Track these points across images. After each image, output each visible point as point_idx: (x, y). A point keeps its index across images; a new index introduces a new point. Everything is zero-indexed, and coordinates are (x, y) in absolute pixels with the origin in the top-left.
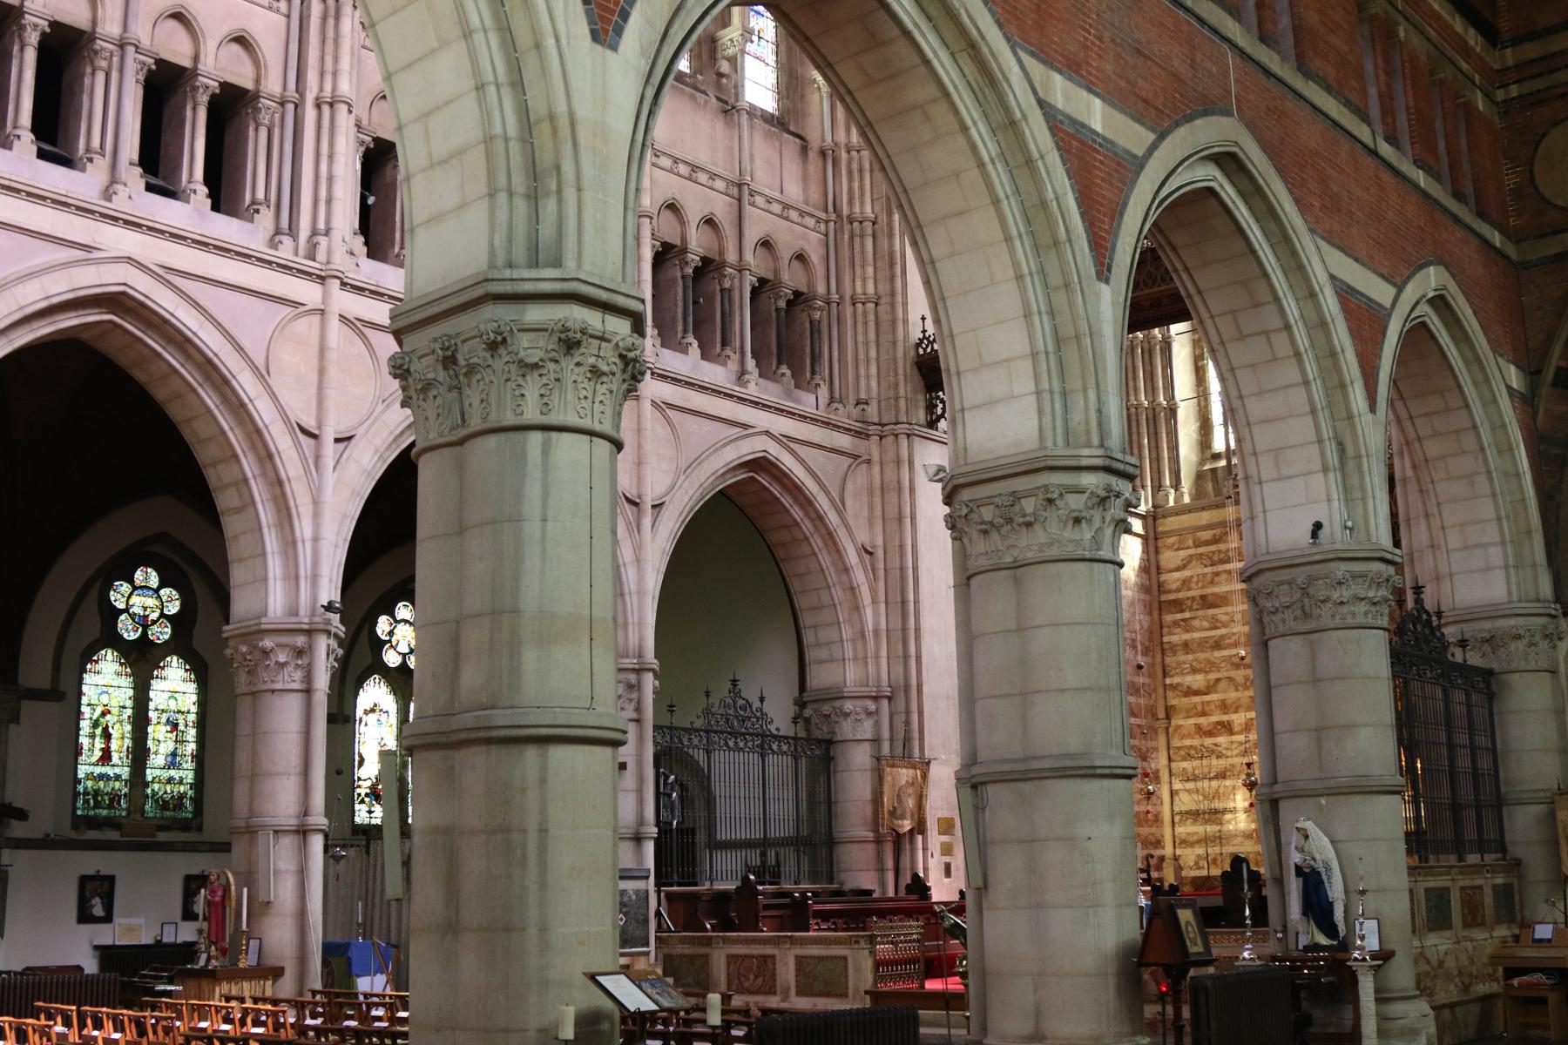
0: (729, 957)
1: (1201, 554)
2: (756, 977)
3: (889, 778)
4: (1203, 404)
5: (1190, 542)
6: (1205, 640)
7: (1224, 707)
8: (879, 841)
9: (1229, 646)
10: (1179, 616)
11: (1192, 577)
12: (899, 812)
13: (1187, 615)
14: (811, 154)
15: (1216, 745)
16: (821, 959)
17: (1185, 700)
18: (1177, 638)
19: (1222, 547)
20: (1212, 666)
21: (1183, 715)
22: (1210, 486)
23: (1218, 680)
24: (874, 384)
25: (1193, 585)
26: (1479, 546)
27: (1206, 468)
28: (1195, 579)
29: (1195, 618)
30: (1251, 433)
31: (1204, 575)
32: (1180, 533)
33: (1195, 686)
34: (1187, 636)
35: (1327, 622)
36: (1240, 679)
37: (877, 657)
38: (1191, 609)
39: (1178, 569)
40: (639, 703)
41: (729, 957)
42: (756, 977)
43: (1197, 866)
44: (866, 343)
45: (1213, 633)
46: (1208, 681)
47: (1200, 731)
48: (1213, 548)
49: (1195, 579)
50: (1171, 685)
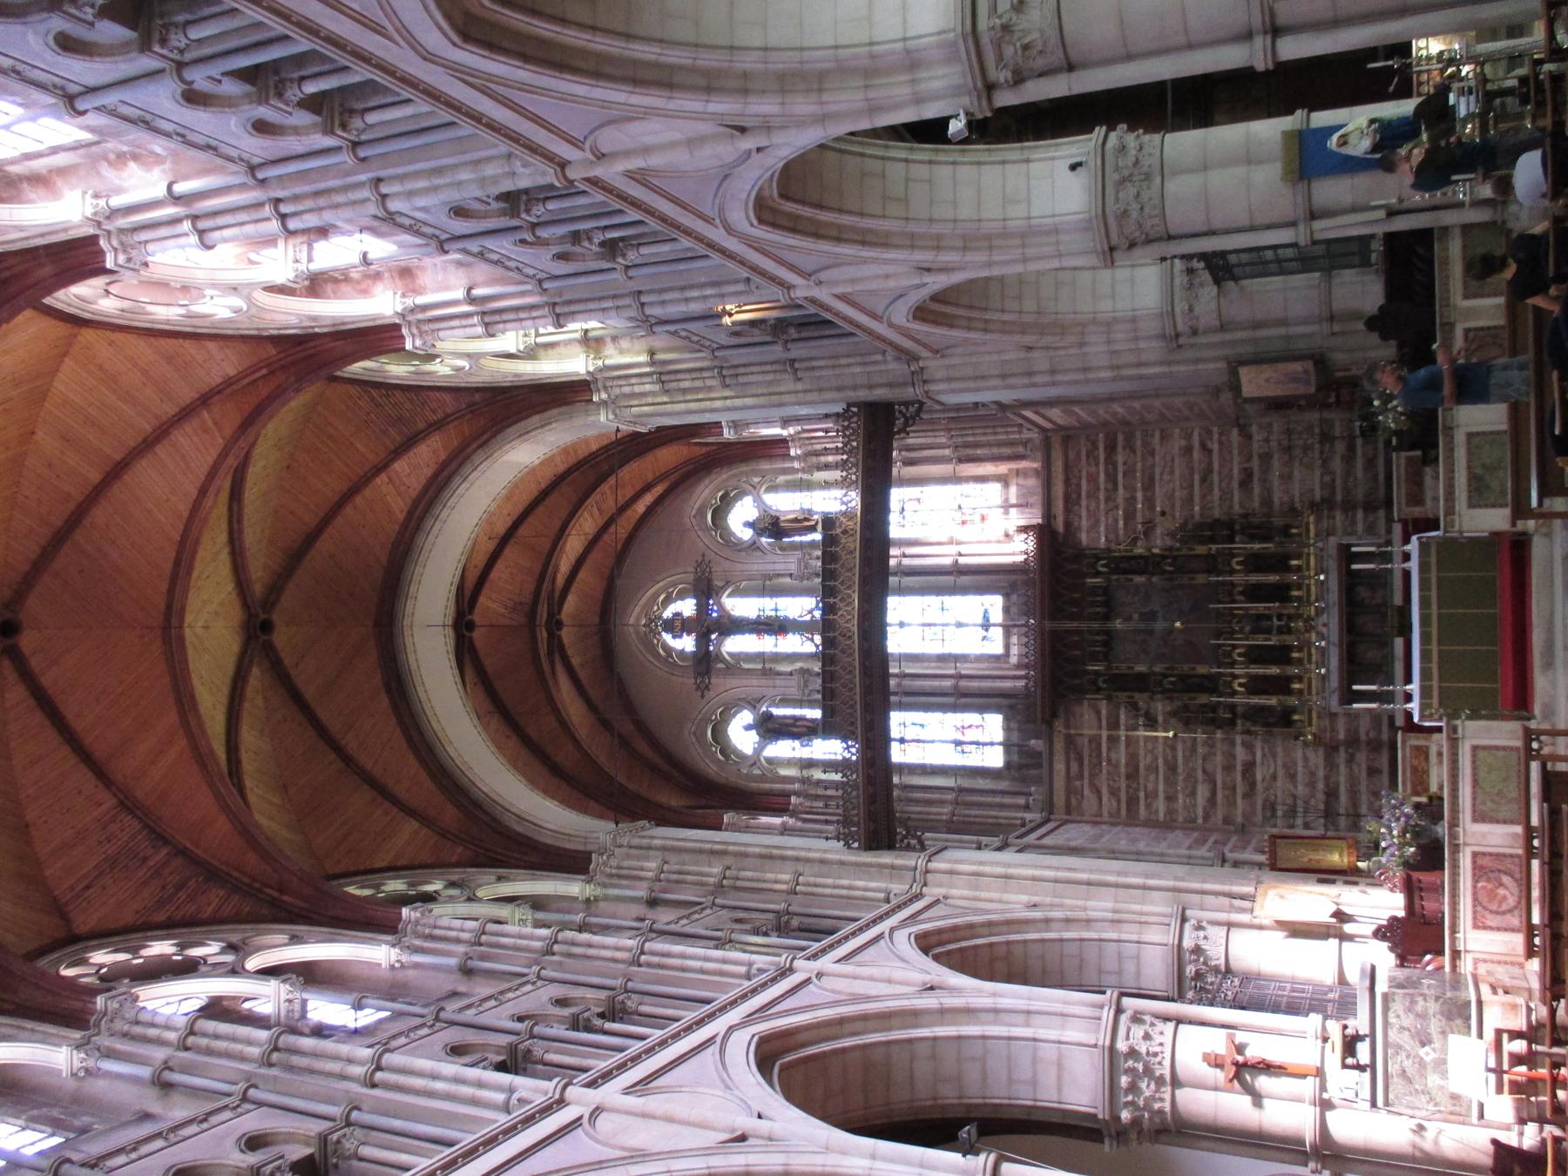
2: (1501, 885)
5: (1078, 783)
6: (1166, 779)
9: (1175, 758)
10: (1142, 802)
11: (1109, 786)
13: (1142, 794)
15: (1263, 780)
17: (1219, 807)
20: (1190, 776)
22: (1033, 772)
23: (1204, 771)
24: (873, 885)
26: (1113, 286)
29: (1146, 787)
30: (989, 220)
31: (1109, 773)
33: (1207, 794)
35: (1155, 161)
37: (1141, 913)
38: (1137, 790)
39: (1100, 799)
40: (1157, 1017)
42: (1501, 885)
44: (835, 887)
45: (1161, 771)
46: (1204, 781)
48: (1086, 762)
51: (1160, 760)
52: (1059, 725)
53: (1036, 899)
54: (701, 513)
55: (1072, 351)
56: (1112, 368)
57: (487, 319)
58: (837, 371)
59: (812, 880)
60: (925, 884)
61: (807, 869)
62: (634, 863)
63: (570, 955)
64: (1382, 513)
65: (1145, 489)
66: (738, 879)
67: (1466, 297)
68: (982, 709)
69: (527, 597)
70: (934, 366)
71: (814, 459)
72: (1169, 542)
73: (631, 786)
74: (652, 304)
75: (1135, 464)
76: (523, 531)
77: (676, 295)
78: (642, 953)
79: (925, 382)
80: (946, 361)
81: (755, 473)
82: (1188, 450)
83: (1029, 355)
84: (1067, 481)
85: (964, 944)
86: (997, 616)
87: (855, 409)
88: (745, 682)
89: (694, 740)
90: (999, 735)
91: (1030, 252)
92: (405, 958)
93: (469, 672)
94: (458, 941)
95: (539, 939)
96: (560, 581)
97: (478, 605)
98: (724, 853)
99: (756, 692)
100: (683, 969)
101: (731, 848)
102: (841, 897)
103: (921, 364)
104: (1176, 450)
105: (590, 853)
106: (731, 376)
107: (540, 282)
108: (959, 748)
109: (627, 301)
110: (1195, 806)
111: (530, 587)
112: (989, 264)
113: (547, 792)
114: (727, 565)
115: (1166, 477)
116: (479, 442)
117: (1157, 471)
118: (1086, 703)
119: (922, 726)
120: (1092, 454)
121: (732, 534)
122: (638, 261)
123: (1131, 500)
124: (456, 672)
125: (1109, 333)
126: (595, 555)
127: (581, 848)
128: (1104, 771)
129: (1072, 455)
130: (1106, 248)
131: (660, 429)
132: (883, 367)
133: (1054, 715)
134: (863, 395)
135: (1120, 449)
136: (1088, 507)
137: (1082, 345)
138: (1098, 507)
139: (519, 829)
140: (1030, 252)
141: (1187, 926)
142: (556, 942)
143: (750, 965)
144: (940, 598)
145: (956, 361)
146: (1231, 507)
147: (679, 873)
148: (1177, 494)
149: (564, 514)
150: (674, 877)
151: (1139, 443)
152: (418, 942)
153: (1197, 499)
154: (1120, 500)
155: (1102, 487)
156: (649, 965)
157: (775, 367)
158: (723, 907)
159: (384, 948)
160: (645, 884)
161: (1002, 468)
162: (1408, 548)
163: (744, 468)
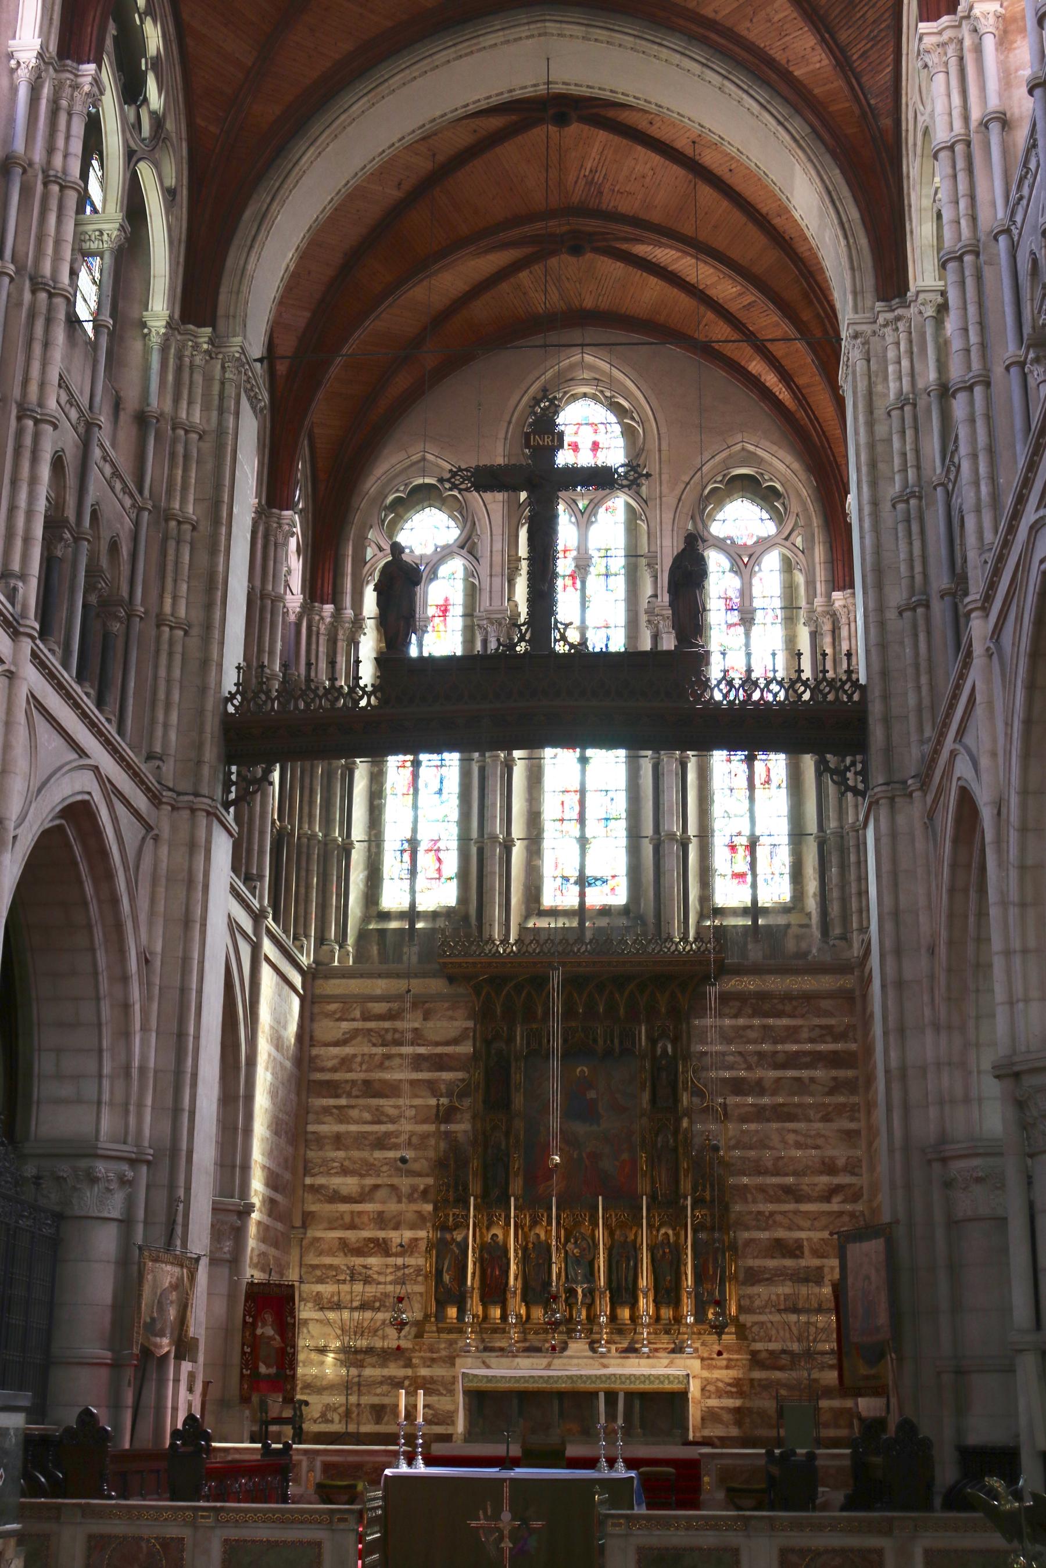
0: (91, 1537)
1: (370, 1030)
3: (150, 1277)
4: (374, 850)
5: (357, 1014)
6: (364, 1135)
7: (381, 1220)
8: (116, 1366)
10: (332, 1102)
11: (355, 1056)
12: (159, 1326)
13: (343, 1101)
14: (123, 416)
15: (365, 1267)
16: (272, 1545)
18: (328, 1128)
19: (398, 1024)
21: (325, 1225)
22: (375, 950)
23: (376, 1187)
24: (173, 736)
25: (355, 1066)
27: (371, 927)
28: (359, 1059)
29: (353, 1107)
31: (372, 1056)
32: (345, 1000)
33: (344, 1191)
34: (342, 1128)
36: (405, 1189)
37: (140, 1106)
38: (349, 1095)
39: (337, 1044)
41: (91, 1537)
43: (324, 1418)
44: (169, 681)
45: (375, 1128)
46: (362, 1187)
47: (345, 1246)
48: (387, 1025)
49: (359, 1059)
50: (312, 1186)
51: (390, 1127)
52: (436, 985)
53: (158, 963)
54: (750, 459)
55: (927, 1012)
56: (903, 1070)
57: (959, 148)
58: (910, 671)
59: (179, 648)
60: (174, 808)
61: (194, 642)
62: (199, 391)
63: (32, 316)
64: (734, 1432)
65: (775, 1107)
66: (178, 543)
67: (927, 1552)
68: (463, 876)
69: (610, 202)
70: (913, 813)
71: (827, 627)
72: (697, 1141)
73: (335, 370)
74: (971, 403)
75: (811, 1094)
76: (706, 193)
77: (982, 439)
78: (37, 422)
79: (892, 800)
80: (919, 833)
81: (809, 540)
82: (829, 1168)
83: (923, 951)
84: (788, 997)
85: (83, 868)
86: (596, 898)
87: (856, 697)
88: (497, 531)
89: (415, 458)
90: (426, 903)
91: (1017, 960)
92: (23, 75)
93: (496, 122)
94: (50, 150)
95: (55, 271)
96: (641, 250)
97: (594, 131)
98: (216, 522)
99: (484, 548)
100: (14, 482)
101: (223, 530)
102: (155, 692)
103: (917, 795)
104: (830, 1152)
105: (213, 325)
106: (908, 511)
107: (1008, 231)
108: (406, 846)
109: (976, 365)
110: (328, 1174)
111: (625, 206)
112: (1004, 904)
113: (307, 255)
114: (671, 500)
115: (791, 1138)
116: (819, 128)
117: (801, 1126)
118: (470, 1024)
119: (440, 792)
120: (828, 1033)
121: (720, 505)
122: (1032, 383)
123: (759, 1088)
124: (483, 105)
125: (949, 1064)
126: (684, 301)
127: (221, 311)
128: (375, 1050)
129: (825, 1004)
130: (1016, 1068)
131: (843, 399)
132: (914, 738)
133: (451, 979)
134: (876, 708)
135: (834, 1073)
136: (750, 1027)
137: (937, 1027)
138: (749, 1042)
139: (247, 214)
140: (1017, 960)
141: (125, 1167)
142: (51, 295)
143: (23, 577)
144: (624, 815)
145: (920, 845)
146: (747, 1228)
147: (186, 457)
148: (768, 1153)
149: (735, 254)
150: (180, 449)
151: (842, 1099)
152: (46, 91)
153: (759, 1180)
154: (759, 1073)
155: (779, 1047)
156: (20, 432)
157: (918, 578)
158: (137, 524)
159: (36, 43)
160: (168, 407)
161: (812, 904)
162: (620, 1465)
163: (816, 522)
